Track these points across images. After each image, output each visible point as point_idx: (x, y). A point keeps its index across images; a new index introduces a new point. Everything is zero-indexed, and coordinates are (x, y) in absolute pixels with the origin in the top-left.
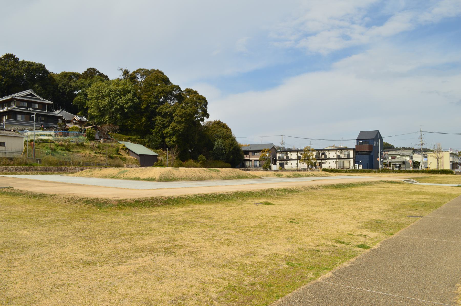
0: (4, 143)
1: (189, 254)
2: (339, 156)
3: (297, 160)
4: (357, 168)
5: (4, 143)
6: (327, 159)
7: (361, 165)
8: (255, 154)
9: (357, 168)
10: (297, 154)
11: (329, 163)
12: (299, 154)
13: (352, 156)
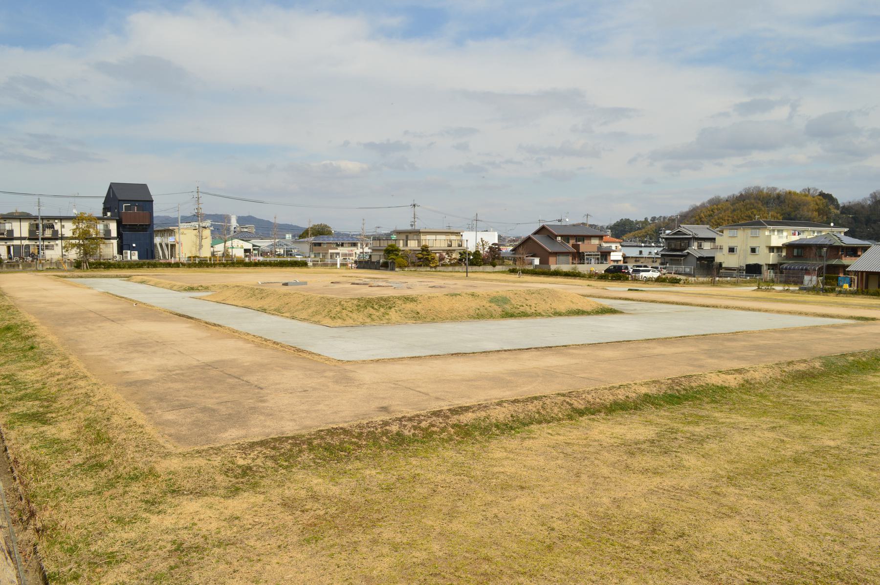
0: (714, 239)
4: (129, 258)
5: (714, 239)
6: (57, 239)
7: (136, 253)
9: (129, 258)
13: (114, 233)
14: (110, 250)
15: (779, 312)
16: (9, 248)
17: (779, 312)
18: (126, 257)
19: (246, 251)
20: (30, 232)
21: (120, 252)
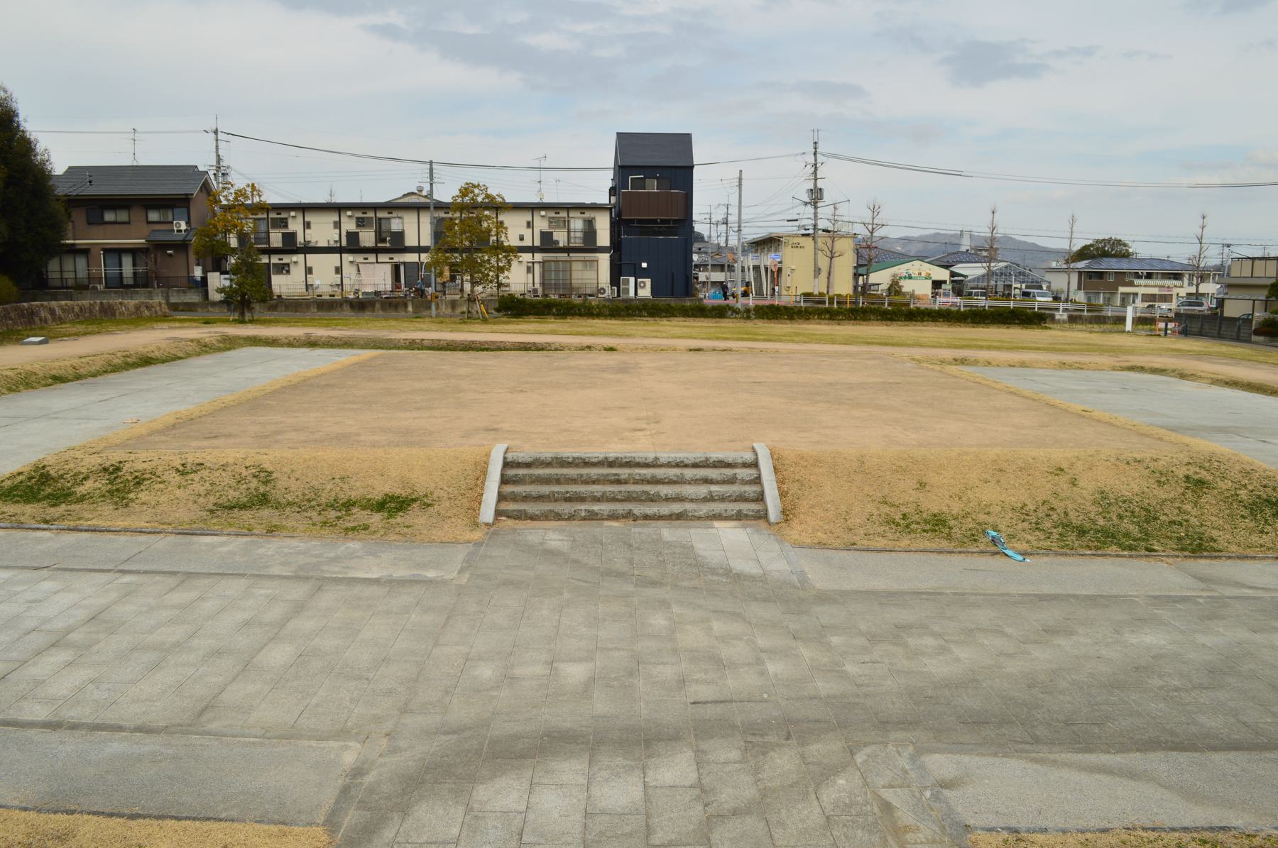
1: (1208, 515)
2: (546, 236)
3: (339, 250)
7: (648, 281)
8: (109, 216)
9: (632, 293)
10: (338, 225)
11: (309, 271)
12: (349, 225)
13: (604, 238)
14: (596, 273)
15: (412, 345)
16: (396, 268)
17: (412, 345)
18: (627, 291)
19: (937, 284)
20: (437, 235)
21: (615, 281)
